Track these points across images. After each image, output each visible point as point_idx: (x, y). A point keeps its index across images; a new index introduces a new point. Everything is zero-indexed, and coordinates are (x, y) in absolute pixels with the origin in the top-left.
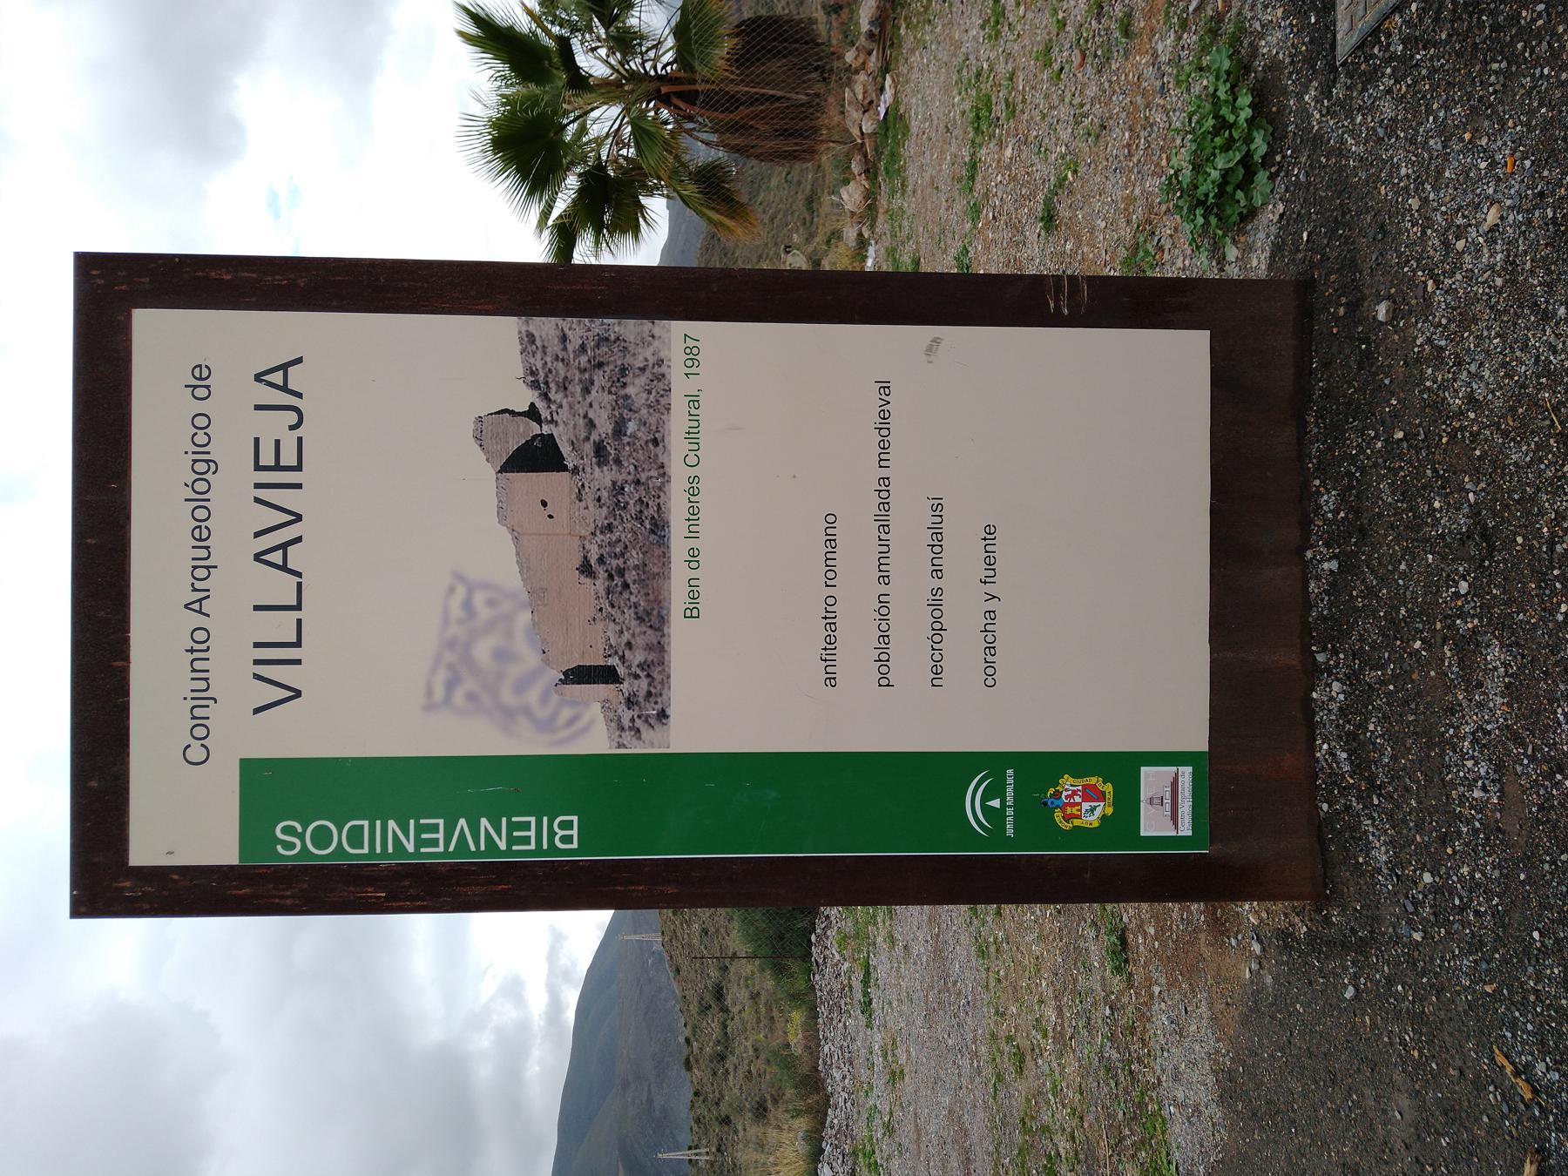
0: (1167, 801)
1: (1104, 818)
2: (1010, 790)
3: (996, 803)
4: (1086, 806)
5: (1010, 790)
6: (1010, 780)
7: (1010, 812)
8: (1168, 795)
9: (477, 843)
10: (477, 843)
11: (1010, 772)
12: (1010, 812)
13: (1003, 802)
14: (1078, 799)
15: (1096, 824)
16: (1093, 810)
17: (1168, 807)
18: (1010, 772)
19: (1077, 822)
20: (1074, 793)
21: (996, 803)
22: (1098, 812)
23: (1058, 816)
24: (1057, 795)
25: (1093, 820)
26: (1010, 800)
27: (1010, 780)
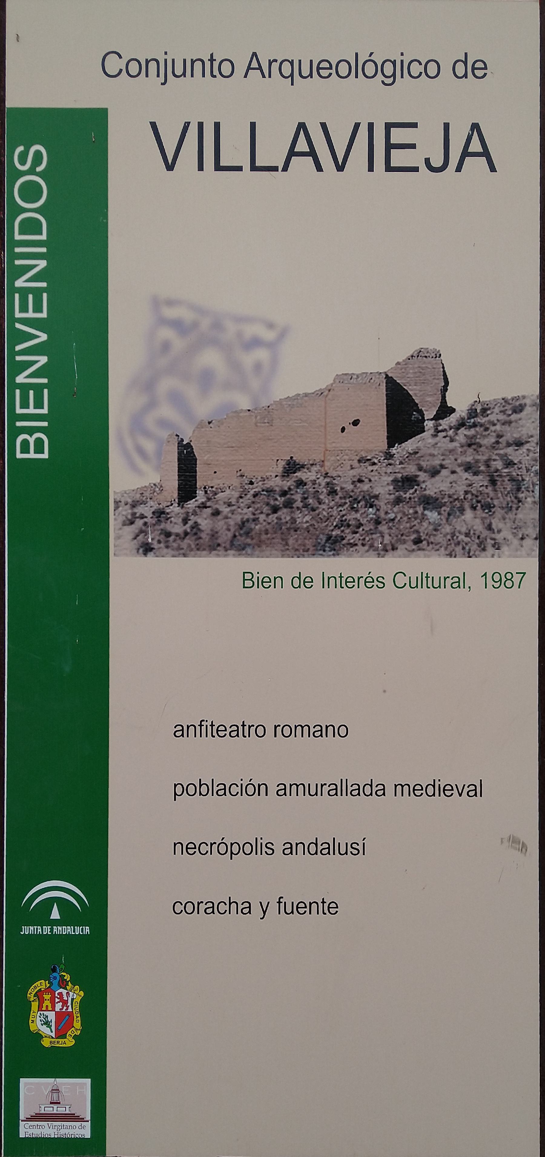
0: (56, 1110)
1: (39, 1036)
2: (68, 930)
3: (55, 914)
4: (52, 1016)
5: (68, 930)
6: (78, 930)
7: (47, 930)
8: (61, 1110)
9: (23, 352)
10: (23, 352)
11: (87, 930)
12: (47, 930)
13: (56, 923)
14: (59, 1006)
15: (32, 1027)
16: (47, 1023)
17: (49, 1110)
18: (87, 930)
19: (35, 1006)
20: (65, 1003)
21: (55, 914)
22: (45, 1030)
23: (42, 984)
24: (63, 984)
25: (36, 1024)
26: (58, 930)
27: (78, 930)
